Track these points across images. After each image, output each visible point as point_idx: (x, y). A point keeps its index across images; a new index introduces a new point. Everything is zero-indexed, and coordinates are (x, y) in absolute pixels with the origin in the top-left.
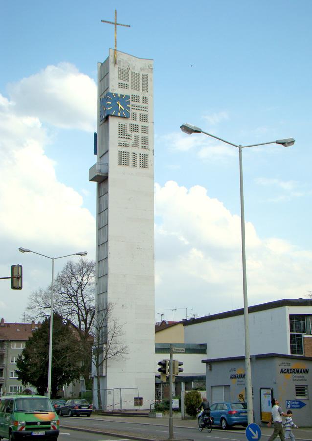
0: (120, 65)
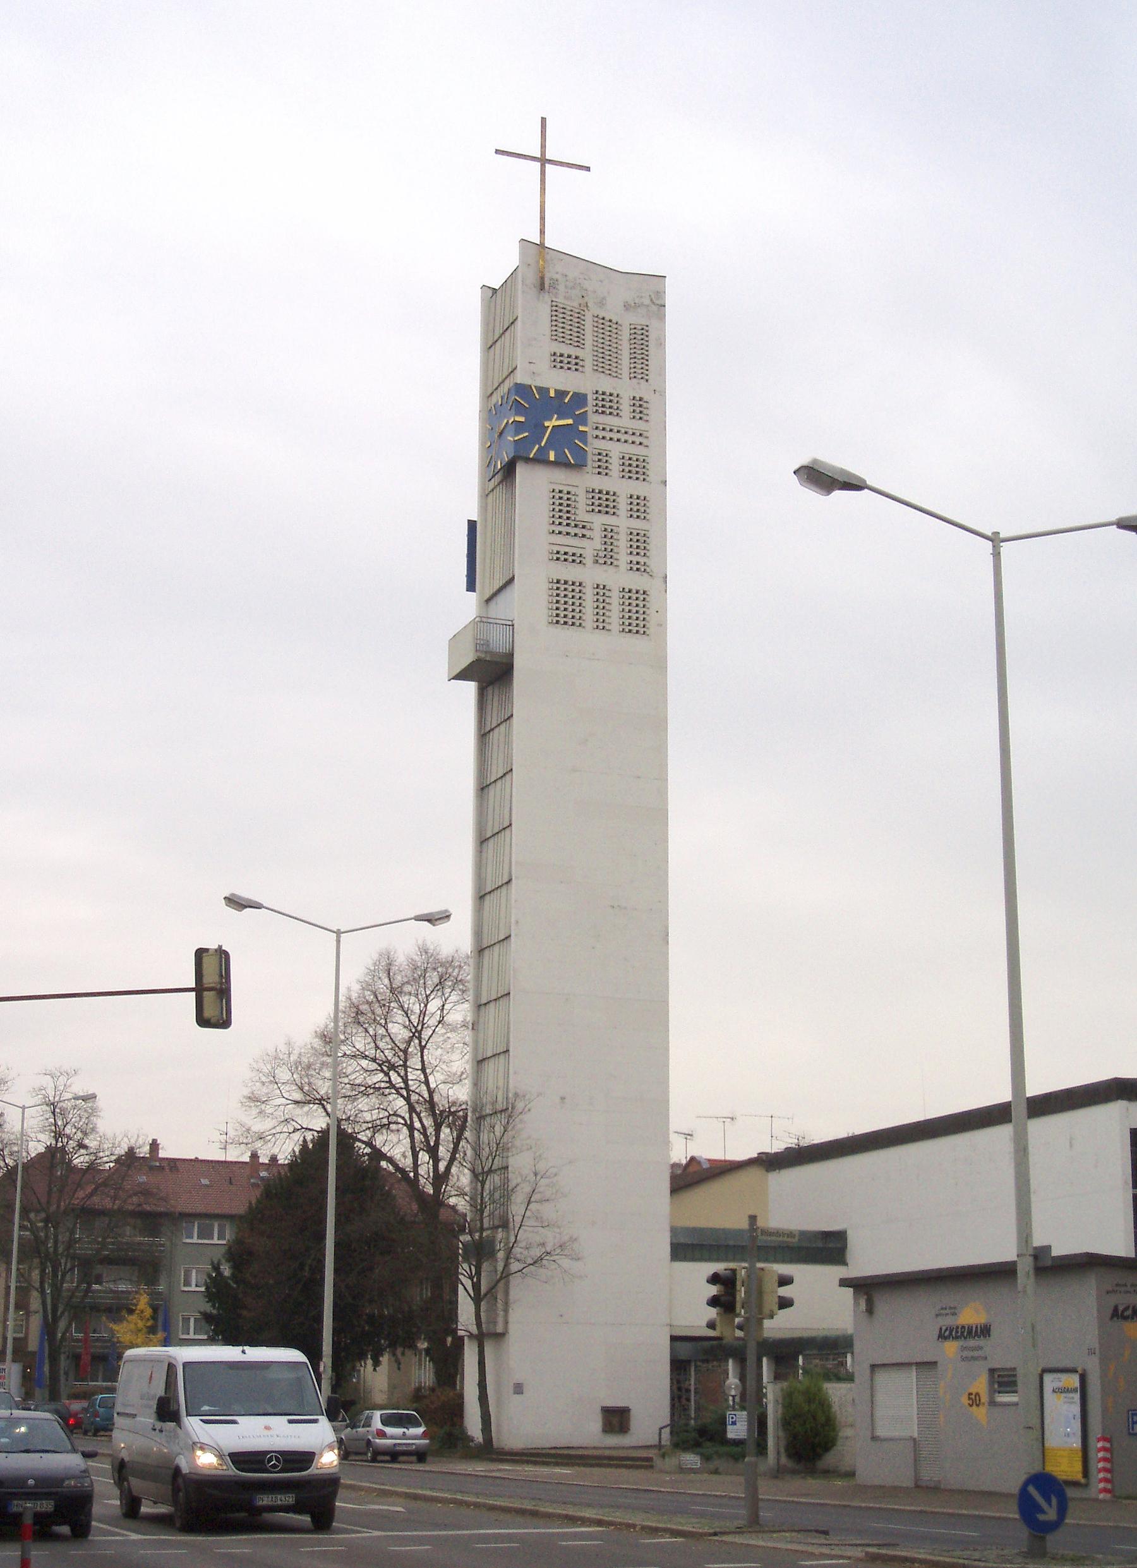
0: (556, 295)
